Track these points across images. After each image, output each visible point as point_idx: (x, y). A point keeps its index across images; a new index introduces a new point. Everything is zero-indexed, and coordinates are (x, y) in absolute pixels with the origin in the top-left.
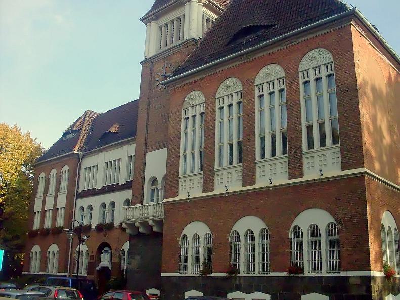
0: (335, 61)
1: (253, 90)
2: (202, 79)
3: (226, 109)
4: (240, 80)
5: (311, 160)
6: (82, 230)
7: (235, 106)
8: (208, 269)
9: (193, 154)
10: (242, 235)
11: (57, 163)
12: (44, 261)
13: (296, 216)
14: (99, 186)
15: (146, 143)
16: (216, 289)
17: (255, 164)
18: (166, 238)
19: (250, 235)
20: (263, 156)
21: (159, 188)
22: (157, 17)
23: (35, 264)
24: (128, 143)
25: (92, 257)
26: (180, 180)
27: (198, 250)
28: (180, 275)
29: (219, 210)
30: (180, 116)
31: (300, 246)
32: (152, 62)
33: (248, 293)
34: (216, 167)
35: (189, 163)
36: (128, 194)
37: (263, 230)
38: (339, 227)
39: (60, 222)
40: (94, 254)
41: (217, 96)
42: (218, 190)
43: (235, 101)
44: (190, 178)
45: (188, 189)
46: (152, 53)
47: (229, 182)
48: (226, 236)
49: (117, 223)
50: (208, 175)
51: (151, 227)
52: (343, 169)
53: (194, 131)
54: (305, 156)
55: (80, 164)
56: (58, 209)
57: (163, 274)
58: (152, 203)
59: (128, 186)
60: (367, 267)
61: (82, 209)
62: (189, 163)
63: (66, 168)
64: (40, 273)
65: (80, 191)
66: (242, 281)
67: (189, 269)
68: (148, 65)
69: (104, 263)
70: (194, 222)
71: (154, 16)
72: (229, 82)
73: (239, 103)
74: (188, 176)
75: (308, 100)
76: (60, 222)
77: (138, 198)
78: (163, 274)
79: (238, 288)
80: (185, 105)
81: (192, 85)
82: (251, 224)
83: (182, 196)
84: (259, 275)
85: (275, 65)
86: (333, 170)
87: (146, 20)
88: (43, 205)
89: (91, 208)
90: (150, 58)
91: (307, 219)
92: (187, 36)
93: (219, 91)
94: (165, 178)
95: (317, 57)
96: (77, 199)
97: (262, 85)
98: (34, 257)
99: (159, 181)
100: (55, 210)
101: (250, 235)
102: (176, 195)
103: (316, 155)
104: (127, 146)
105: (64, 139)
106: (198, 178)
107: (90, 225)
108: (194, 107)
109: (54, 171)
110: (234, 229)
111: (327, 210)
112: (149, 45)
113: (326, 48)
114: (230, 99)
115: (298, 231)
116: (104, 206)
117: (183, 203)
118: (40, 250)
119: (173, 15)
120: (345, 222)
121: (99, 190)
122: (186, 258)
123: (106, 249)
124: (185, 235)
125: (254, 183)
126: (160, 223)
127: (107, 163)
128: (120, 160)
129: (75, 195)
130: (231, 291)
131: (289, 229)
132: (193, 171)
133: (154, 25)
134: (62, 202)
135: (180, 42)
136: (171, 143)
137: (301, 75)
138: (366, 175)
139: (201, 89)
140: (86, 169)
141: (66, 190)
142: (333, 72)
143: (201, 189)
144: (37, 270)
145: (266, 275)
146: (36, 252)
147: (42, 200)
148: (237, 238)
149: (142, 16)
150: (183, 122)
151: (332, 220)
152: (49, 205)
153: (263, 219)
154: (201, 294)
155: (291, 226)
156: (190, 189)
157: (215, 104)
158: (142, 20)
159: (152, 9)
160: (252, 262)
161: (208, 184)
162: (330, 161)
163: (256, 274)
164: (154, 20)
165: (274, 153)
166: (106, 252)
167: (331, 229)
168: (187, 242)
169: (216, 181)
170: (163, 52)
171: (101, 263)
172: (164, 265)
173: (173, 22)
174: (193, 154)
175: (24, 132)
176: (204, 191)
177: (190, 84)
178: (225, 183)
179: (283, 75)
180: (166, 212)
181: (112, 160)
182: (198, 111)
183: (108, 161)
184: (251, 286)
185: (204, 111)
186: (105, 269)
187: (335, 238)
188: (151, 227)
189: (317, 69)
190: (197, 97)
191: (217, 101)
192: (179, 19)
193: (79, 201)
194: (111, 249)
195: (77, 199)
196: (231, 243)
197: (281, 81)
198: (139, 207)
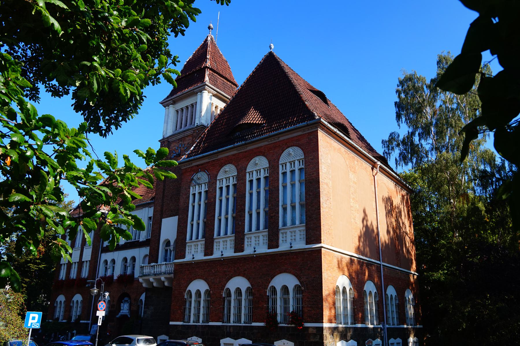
0: (305, 158)
1: (245, 176)
3: (289, 175)
4: (236, 166)
7: (297, 172)
9: (198, 224)
12: (68, 308)
13: (272, 278)
16: (211, 337)
17: (244, 235)
19: (238, 291)
20: (250, 230)
21: (172, 249)
22: (174, 103)
23: (60, 312)
27: (240, 302)
28: (185, 324)
29: (217, 272)
30: (189, 191)
31: (275, 302)
32: (169, 141)
33: (236, 339)
36: (146, 251)
37: (248, 288)
38: (303, 288)
39: (85, 273)
41: (218, 178)
42: (248, 251)
43: (297, 167)
44: (195, 243)
45: (193, 253)
46: (170, 133)
47: (224, 249)
48: (220, 292)
51: (152, 283)
52: (307, 243)
54: (280, 232)
57: (171, 323)
58: (164, 263)
60: (320, 320)
61: (106, 262)
66: (231, 329)
69: (124, 311)
73: (300, 170)
75: (285, 187)
77: (153, 258)
78: (171, 323)
79: (229, 335)
82: (238, 283)
83: (188, 258)
84: (194, 324)
85: (262, 157)
86: (300, 245)
89: (113, 261)
90: (168, 138)
92: (197, 122)
93: (219, 174)
94: (176, 241)
95: (293, 153)
97: (252, 172)
98: (59, 306)
99: (172, 243)
100: (81, 263)
101: (238, 291)
102: (184, 257)
103: (288, 231)
106: (300, 231)
110: (188, 289)
111: (294, 275)
112: (167, 126)
113: (300, 148)
114: (284, 167)
115: (274, 290)
117: (189, 265)
119: (188, 102)
122: (190, 309)
123: (126, 299)
124: (189, 291)
125: (243, 251)
130: (224, 337)
131: (267, 288)
133: (172, 109)
135: (192, 127)
136: (181, 213)
137: (280, 167)
138: (323, 249)
142: (303, 167)
145: (249, 325)
146: (61, 302)
147: (80, 251)
148: (229, 294)
150: (191, 197)
153: (249, 279)
154: (250, 342)
155: (268, 286)
156: (195, 253)
157: (216, 184)
158: (162, 103)
159: (168, 97)
160: (238, 313)
161: (209, 250)
163: (243, 324)
165: (258, 228)
166: (127, 301)
167: (297, 288)
168: (191, 297)
169: (215, 247)
171: (121, 311)
173: (187, 107)
174: (258, 214)
176: (205, 255)
178: (221, 249)
179: (268, 166)
182: (231, 183)
184: (237, 333)
186: (124, 316)
187: (300, 296)
188: (152, 283)
189: (284, 165)
191: (218, 182)
192: (192, 105)
193: (103, 255)
194: (130, 298)
196: (224, 298)
197: (301, 161)
198: (166, 264)
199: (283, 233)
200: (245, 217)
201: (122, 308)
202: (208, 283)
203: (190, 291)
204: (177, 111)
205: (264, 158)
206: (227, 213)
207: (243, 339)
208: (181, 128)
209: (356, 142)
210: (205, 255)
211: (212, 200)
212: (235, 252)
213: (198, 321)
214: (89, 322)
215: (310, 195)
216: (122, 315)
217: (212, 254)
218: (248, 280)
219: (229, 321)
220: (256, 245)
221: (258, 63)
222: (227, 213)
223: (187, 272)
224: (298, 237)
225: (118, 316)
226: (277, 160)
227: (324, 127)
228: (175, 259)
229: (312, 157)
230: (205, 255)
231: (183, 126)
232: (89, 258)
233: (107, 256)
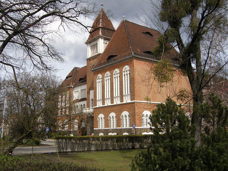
10: (111, 117)
12: (107, 123)
18: (94, 118)
24: (84, 84)
35: (99, 96)
37: (116, 116)
50: (122, 97)
51: (91, 115)
52: (131, 100)
53: (117, 82)
64: (106, 128)
72: (107, 73)
74: (108, 99)
82: (113, 114)
83: (98, 106)
88: (134, 84)
101: (147, 115)
108: (100, 79)
115: (143, 116)
116: (82, 105)
125: (113, 103)
126: (93, 113)
132: (118, 95)
156: (99, 104)
158: (86, 43)
161: (122, 100)
172: (94, 126)
176: (103, 105)
177: (98, 71)
180: (94, 111)
181: (83, 89)
190: (100, 76)
191: (105, 78)
200: (113, 91)
204: (91, 46)
206: (127, 85)
207: (145, 133)
209: (145, 56)
210: (103, 105)
213: (114, 127)
218: (115, 113)
219: (111, 127)
220: (117, 101)
222: (127, 85)
223: (98, 110)
230: (131, 100)
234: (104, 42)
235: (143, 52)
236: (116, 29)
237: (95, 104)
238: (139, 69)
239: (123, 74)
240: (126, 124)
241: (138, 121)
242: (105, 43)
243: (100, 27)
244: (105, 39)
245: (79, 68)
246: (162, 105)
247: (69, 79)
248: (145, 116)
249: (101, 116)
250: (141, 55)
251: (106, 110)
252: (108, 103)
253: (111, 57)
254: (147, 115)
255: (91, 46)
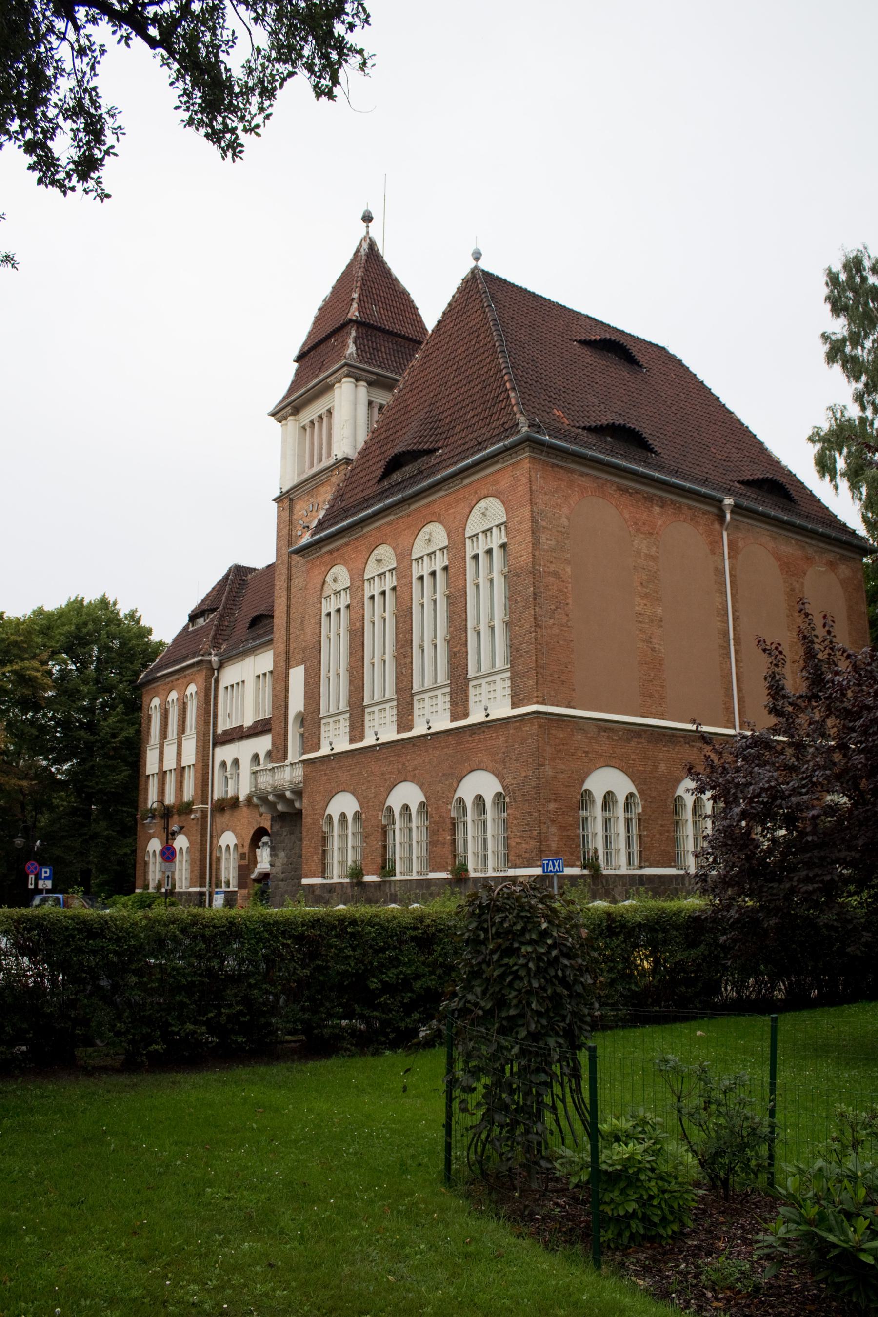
2: (347, 544)
5: (478, 691)
6: (229, 805)
8: (356, 874)
11: (178, 679)
14: (248, 722)
15: (287, 653)
18: (307, 820)
23: (227, 868)
25: (242, 856)
26: (472, 684)
32: (291, 500)
34: (471, 673)
35: (334, 696)
36: (263, 744)
39: (188, 794)
40: (246, 850)
41: (366, 577)
42: (476, 717)
49: (242, 798)
55: (217, 681)
56: (184, 768)
59: (260, 729)
61: (224, 764)
62: (334, 696)
63: (192, 689)
65: (219, 731)
67: (336, 872)
68: (286, 503)
70: (340, 794)
71: (289, 408)
76: (188, 794)
78: (305, 881)
80: (327, 591)
81: (335, 554)
82: (407, 795)
83: (324, 751)
87: (279, 414)
89: (236, 762)
90: (287, 492)
91: (481, 785)
96: (214, 746)
100: (181, 770)
101: (609, 799)
102: (318, 748)
104: (252, 657)
105: (191, 629)
107: (238, 798)
109: (173, 695)
110: (326, 813)
115: (586, 798)
118: (188, 845)
120: (514, 792)
121: (250, 728)
124: (329, 815)
126: (298, 793)
127: (259, 677)
128: (243, 682)
129: (213, 738)
131: (451, 803)
132: (493, 666)
134: (189, 757)
139: (345, 563)
140: (227, 688)
141: (194, 731)
143: (395, 727)
144: (185, 883)
149: (271, 406)
151: (501, 790)
152: (170, 763)
156: (336, 739)
161: (459, 707)
162: (499, 693)
164: (292, 414)
166: (265, 844)
167: (357, 815)
170: (307, 480)
171: (259, 866)
175: (123, 610)
176: (514, 705)
183: (260, 673)
185: (505, 540)
193: (218, 750)
195: (214, 746)
199: (419, 701)
201: (259, 859)
202: (357, 798)
203: (461, 800)
205: (440, 526)
208: (320, 460)
211: (358, 625)
212: (398, 732)
214: (203, 889)
215: (516, 602)
216: (260, 874)
217: (466, 715)
218: (421, 787)
220: (434, 717)
221: (449, 299)
223: (326, 771)
224: (499, 693)
225: (253, 876)
226: (460, 530)
227: (541, 447)
228: (303, 753)
229: (519, 519)
230: (514, 705)
231: (324, 457)
232: (192, 761)
233: (225, 754)
234: (370, 403)
235: (584, 428)
236: (431, 315)
237: (311, 741)
238: (564, 521)
239: (469, 553)
240: (486, 856)
241: (553, 830)
242: (376, 410)
243: (351, 321)
244: (376, 383)
245: (255, 569)
246: (300, 712)
247: (201, 621)
248: (599, 802)
249: (344, 804)
250: (575, 440)
251: (373, 767)
252: (382, 729)
253: (395, 463)
254: (609, 799)
255: (304, 428)
